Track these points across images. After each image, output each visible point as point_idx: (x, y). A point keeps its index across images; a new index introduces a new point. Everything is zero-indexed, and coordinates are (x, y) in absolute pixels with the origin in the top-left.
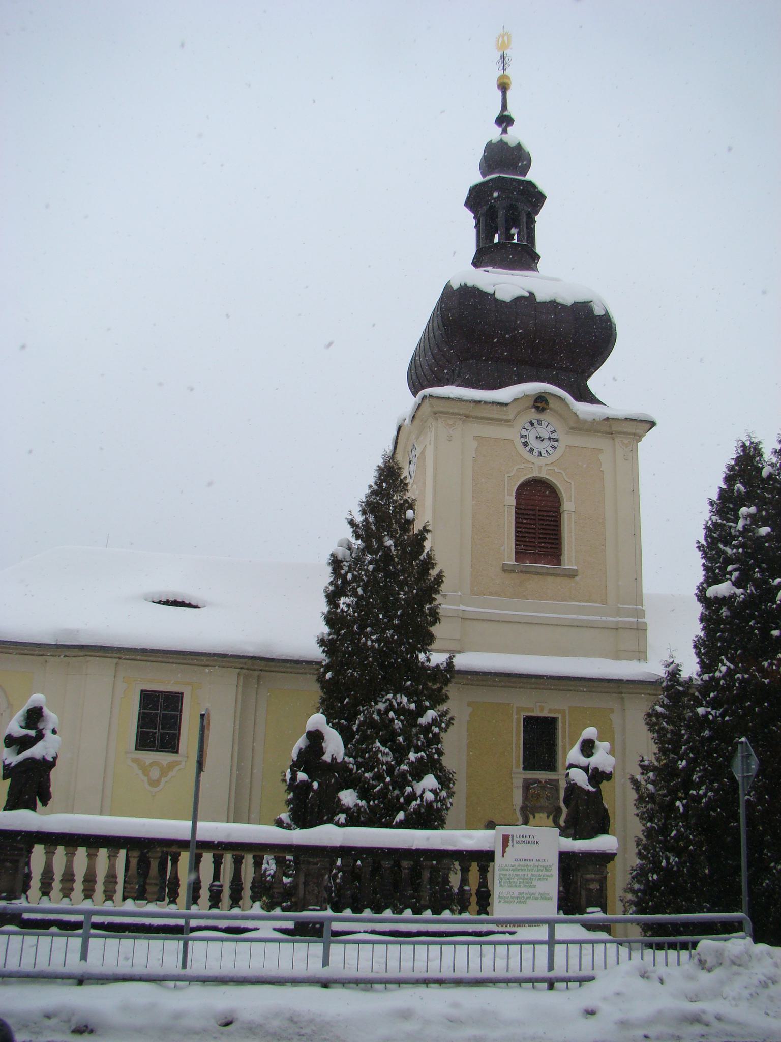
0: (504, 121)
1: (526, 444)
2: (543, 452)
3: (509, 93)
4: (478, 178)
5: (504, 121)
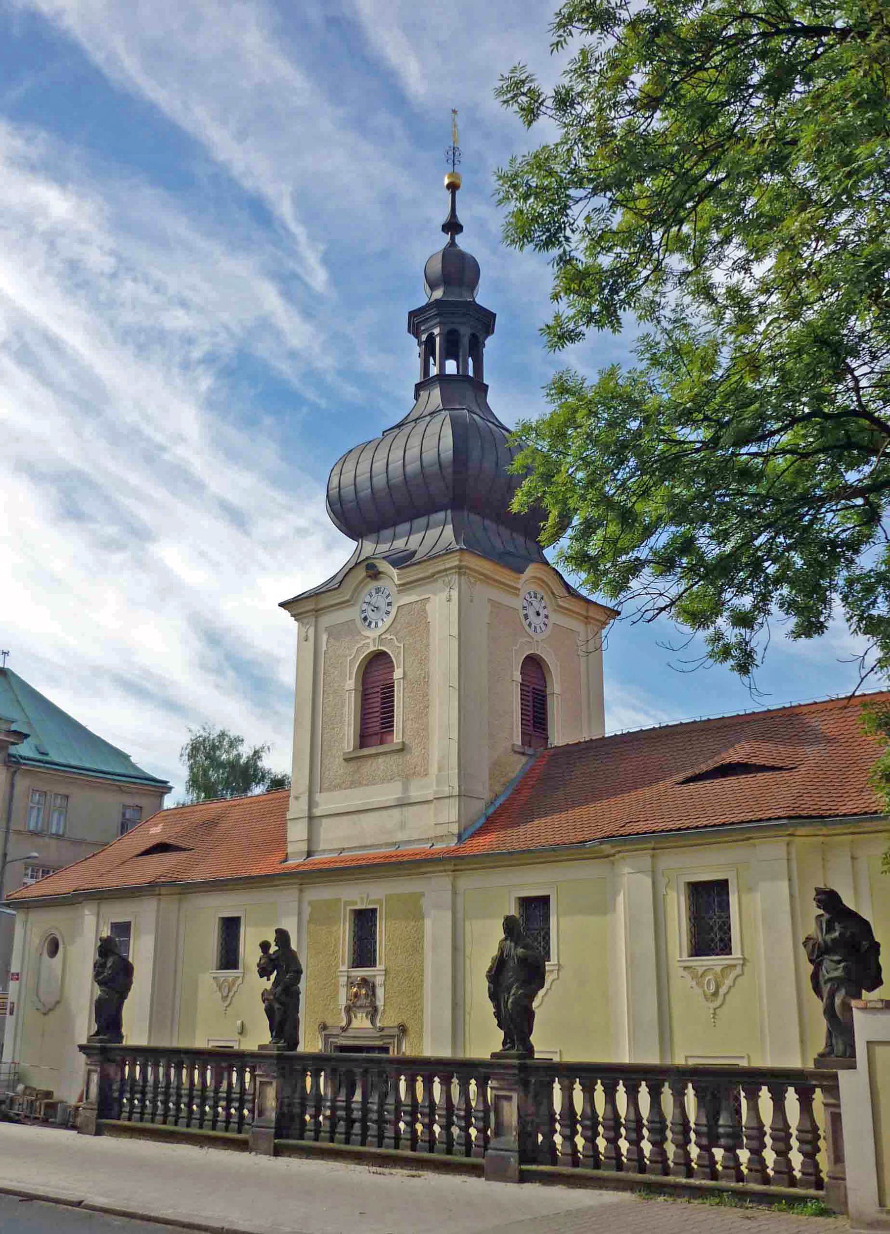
0: (453, 227)
1: (526, 617)
2: (538, 628)
3: (458, 193)
4: (422, 297)
5: (453, 227)
